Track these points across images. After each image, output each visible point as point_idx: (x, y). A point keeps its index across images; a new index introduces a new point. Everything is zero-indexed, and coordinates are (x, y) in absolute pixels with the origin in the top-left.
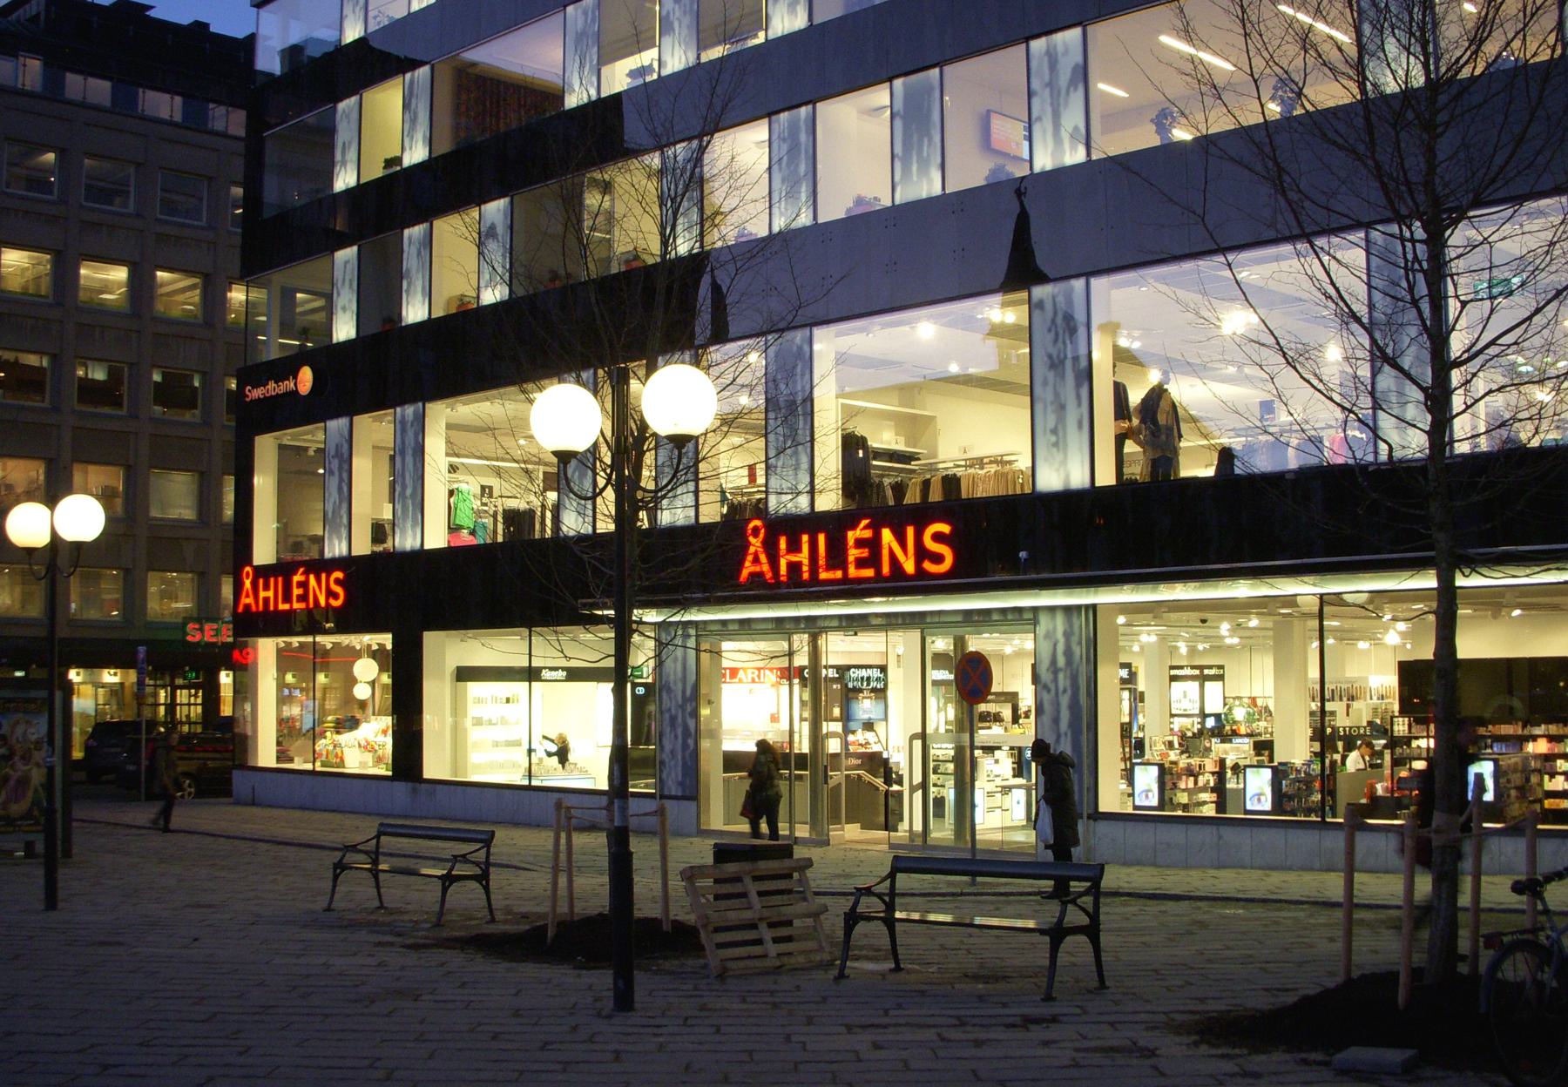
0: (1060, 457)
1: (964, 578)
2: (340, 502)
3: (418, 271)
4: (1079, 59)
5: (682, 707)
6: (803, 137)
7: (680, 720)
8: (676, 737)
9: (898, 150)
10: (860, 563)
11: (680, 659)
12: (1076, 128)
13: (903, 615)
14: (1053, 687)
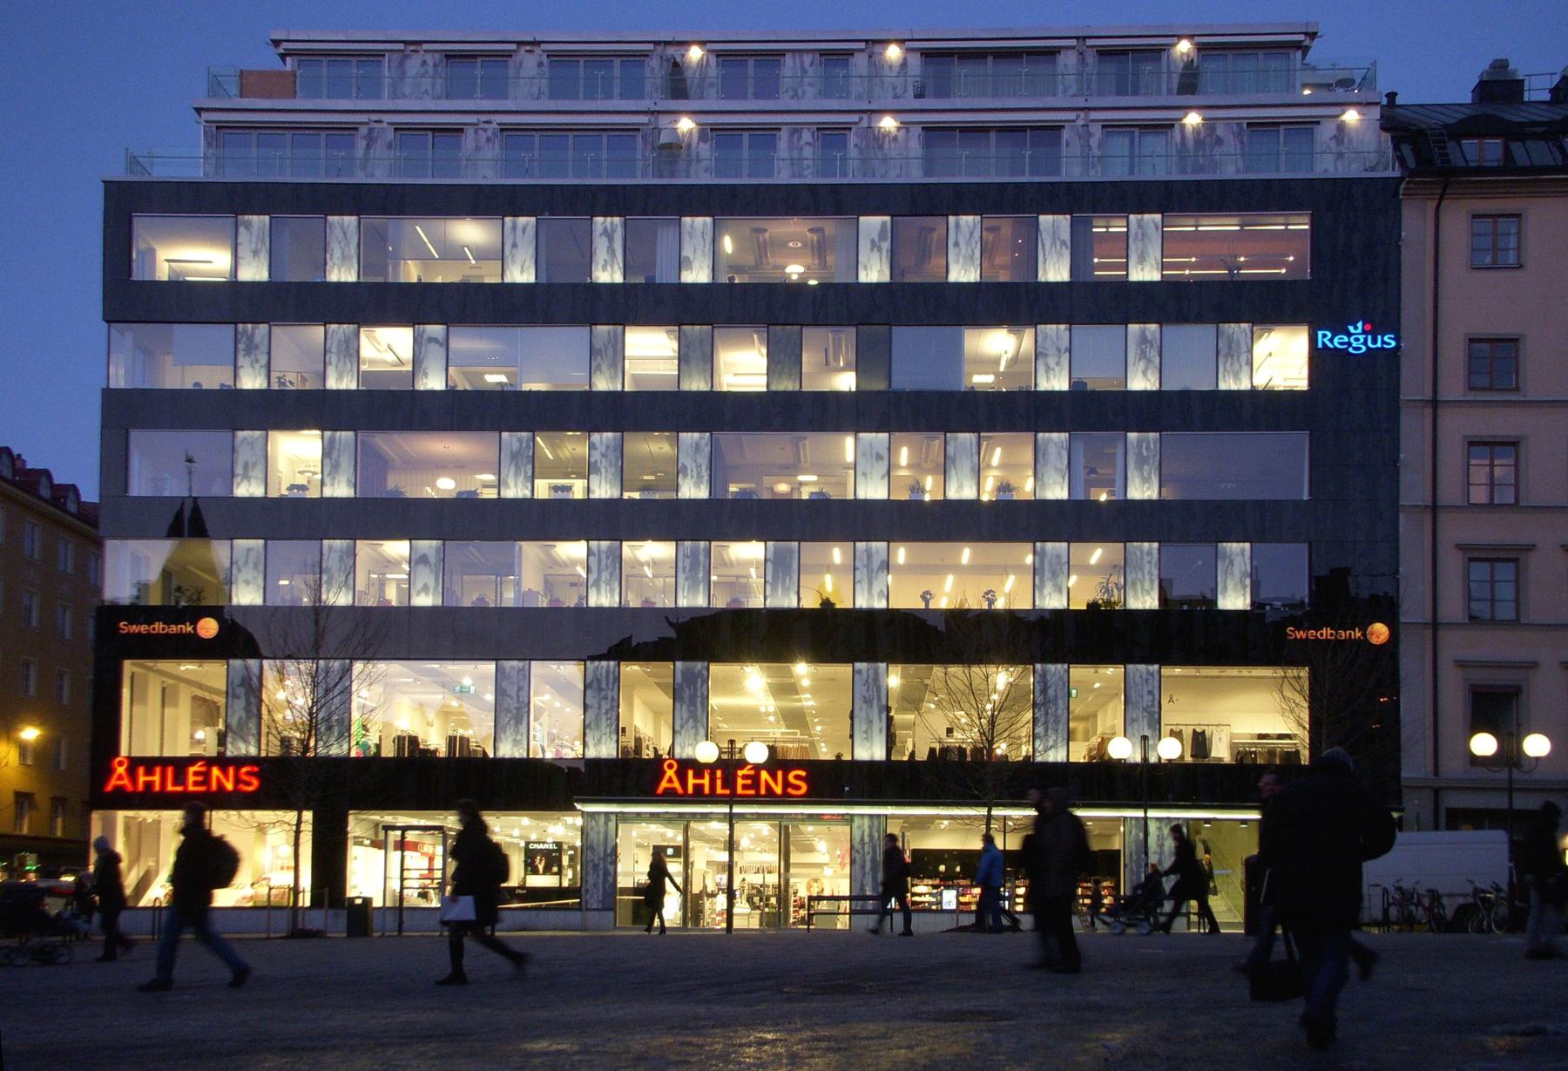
0: (868, 745)
1: (813, 797)
2: (248, 718)
4: (885, 557)
6: (702, 558)
7: (601, 866)
8: (598, 876)
9: (769, 578)
12: (881, 591)
13: (769, 814)
14: (861, 851)
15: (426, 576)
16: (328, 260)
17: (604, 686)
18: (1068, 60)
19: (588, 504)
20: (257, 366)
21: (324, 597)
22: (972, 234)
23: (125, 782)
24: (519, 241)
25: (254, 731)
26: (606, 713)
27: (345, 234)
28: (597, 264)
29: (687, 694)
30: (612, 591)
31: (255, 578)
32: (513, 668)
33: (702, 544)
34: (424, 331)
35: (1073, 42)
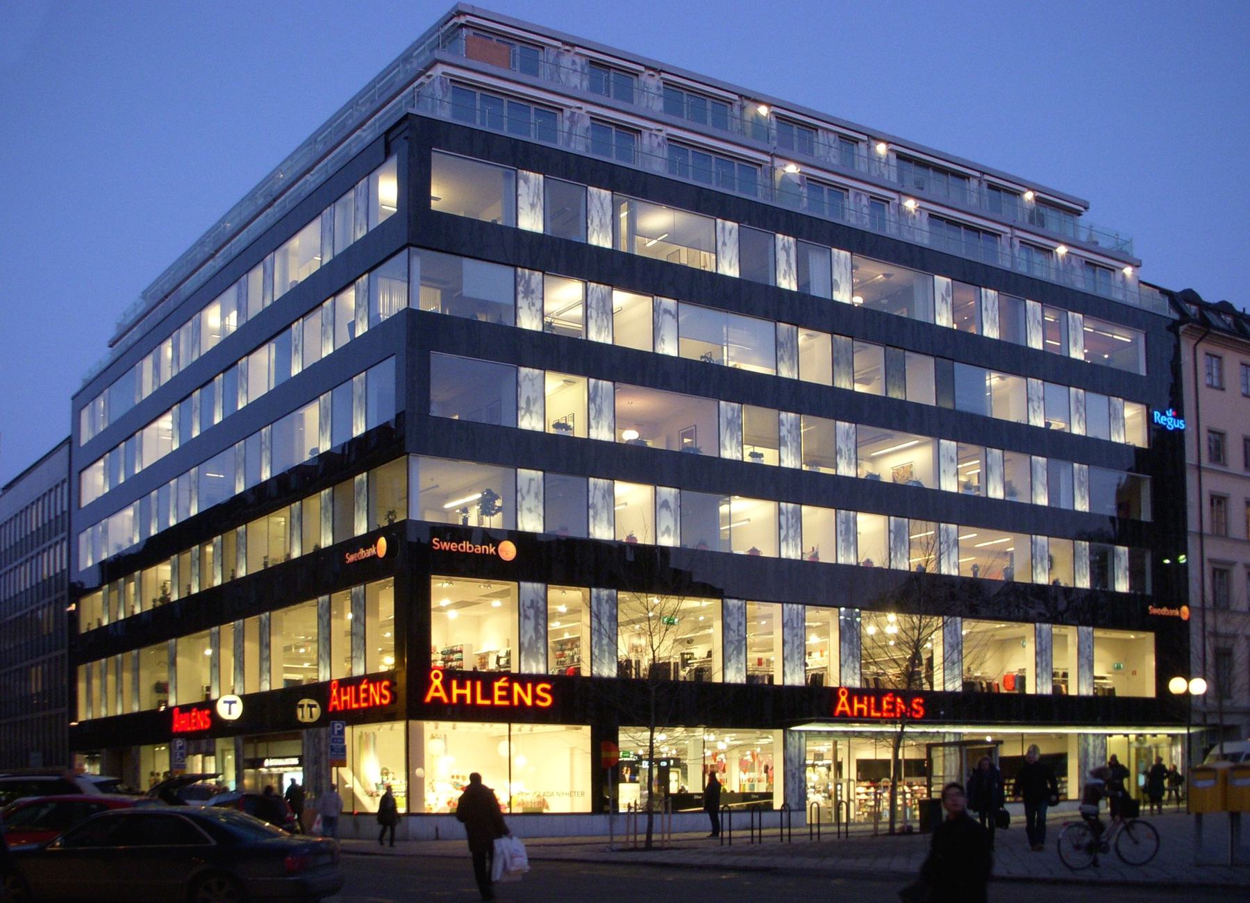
2: (537, 638)
3: (603, 507)
5: (799, 769)
10: (501, 698)
11: (797, 747)
15: (668, 520)
16: (589, 225)
17: (795, 625)
18: (974, 183)
19: (778, 471)
20: (533, 309)
21: (591, 530)
22: (994, 303)
23: (442, 694)
24: (728, 242)
25: (542, 650)
26: (797, 648)
27: (602, 205)
28: (780, 272)
29: (848, 635)
30: (796, 546)
31: (536, 507)
32: (734, 606)
33: (852, 513)
34: (661, 303)
35: (978, 174)
